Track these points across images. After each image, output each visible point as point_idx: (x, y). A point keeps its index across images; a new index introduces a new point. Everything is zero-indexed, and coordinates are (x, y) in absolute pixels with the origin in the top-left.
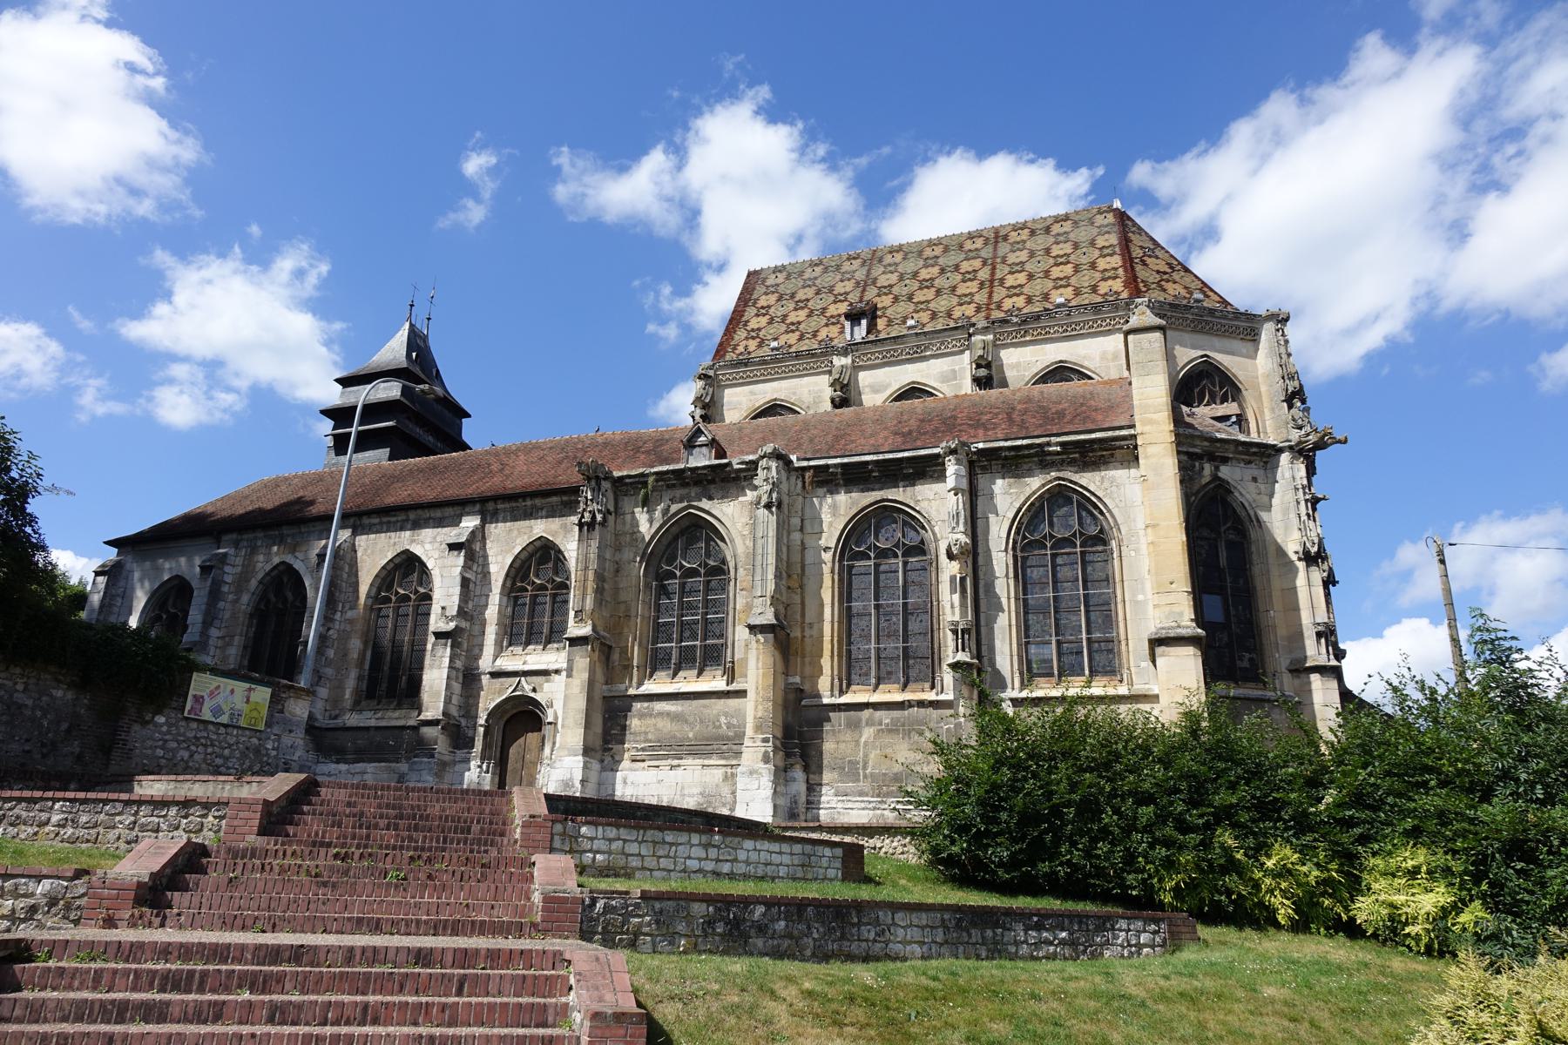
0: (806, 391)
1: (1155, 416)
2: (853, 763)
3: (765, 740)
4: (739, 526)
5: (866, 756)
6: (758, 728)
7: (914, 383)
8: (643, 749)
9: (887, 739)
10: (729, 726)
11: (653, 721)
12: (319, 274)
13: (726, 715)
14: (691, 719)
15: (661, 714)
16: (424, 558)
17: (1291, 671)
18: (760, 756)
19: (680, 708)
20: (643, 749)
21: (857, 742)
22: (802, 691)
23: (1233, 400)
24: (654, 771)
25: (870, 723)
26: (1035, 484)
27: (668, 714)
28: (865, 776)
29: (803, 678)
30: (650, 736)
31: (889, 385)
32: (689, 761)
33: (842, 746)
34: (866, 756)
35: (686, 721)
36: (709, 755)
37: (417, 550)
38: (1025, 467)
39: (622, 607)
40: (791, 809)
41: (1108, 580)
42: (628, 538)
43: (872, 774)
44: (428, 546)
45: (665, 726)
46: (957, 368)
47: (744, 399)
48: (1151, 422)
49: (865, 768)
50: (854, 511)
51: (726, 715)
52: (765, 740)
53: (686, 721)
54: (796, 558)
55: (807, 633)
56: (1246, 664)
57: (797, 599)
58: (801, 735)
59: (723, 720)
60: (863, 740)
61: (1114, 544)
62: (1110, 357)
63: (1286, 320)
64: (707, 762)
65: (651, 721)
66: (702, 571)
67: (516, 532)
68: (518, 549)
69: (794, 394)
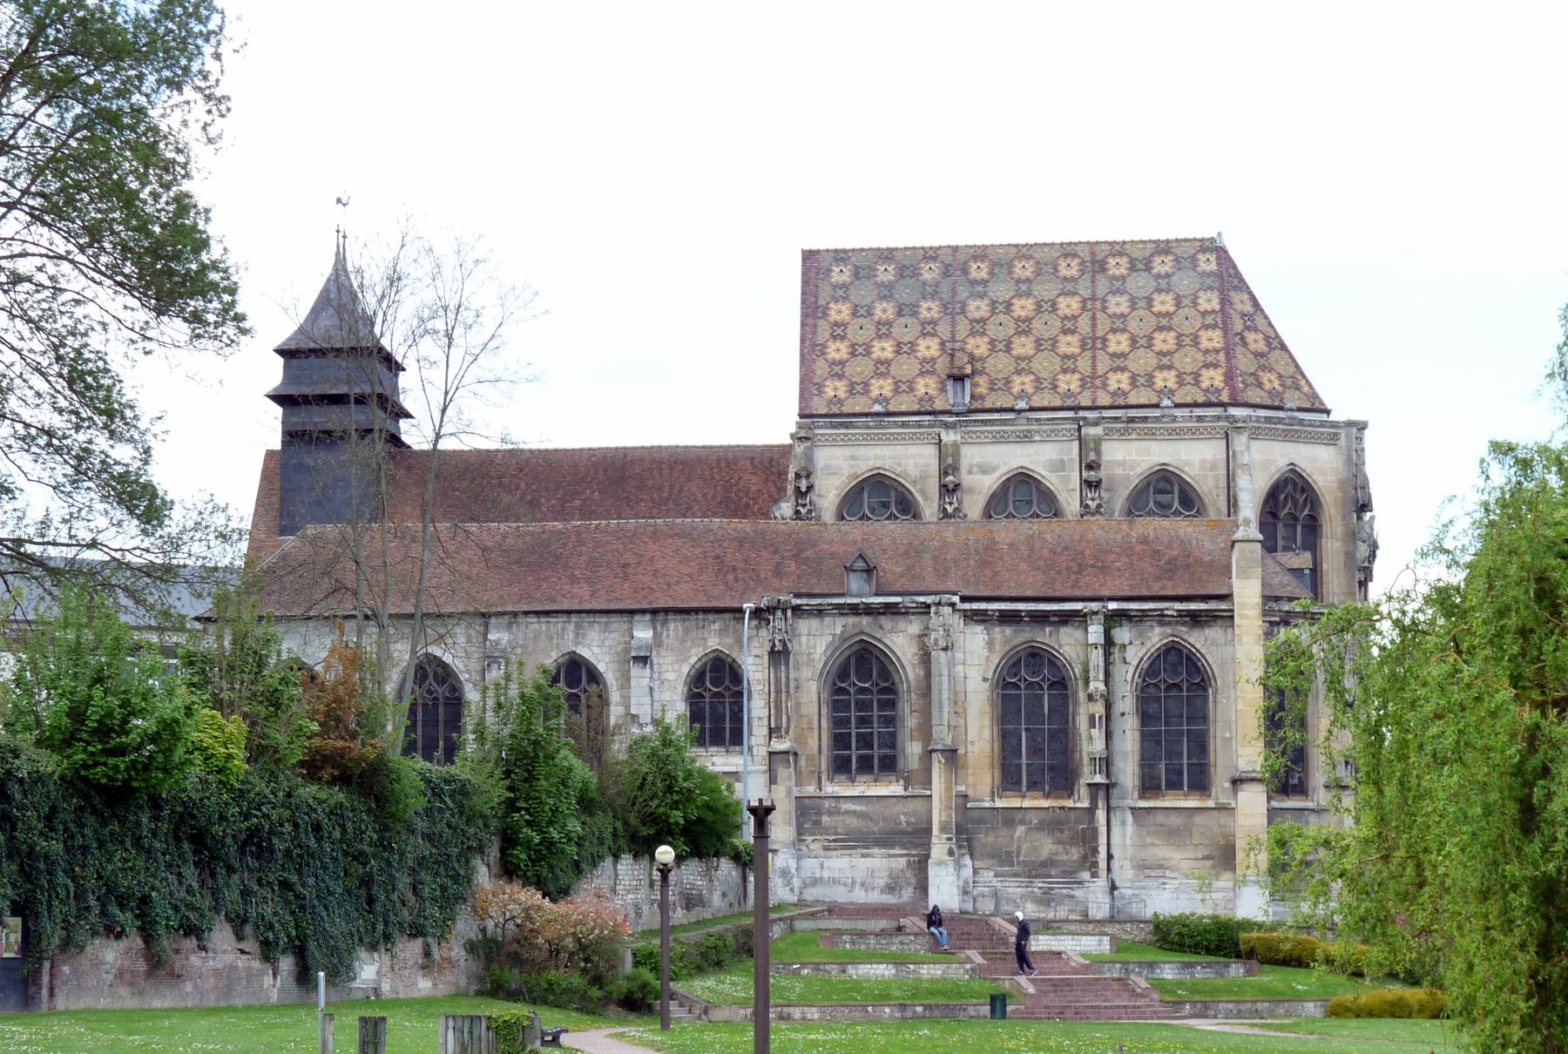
0: (911, 462)
1: (1250, 613)
2: (1009, 853)
3: (949, 839)
4: (909, 656)
5: (1019, 847)
6: (943, 829)
7: (1022, 467)
8: (834, 841)
9: (1037, 835)
10: (908, 823)
11: (841, 818)
12: (1249, 973)
13: (905, 814)
14: (875, 817)
15: (847, 812)
16: (592, 660)
17: (1326, 787)
18: (946, 851)
19: (864, 808)
20: (834, 841)
21: (1012, 838)
22: (966, 796)
23: (1305, 548)
24: (847, 859)
25: (1022, 822)
26: (1157, 637)
27: (854, 812)
28: (1018, 863)
29: (967, 786)
30: (839, 830)
31: (996, 469)
32: (876, 851)
33: (1000, 840)
34: (1019, 847)
35: (871, 819)
36: (892, 846)
37: (585, 652)
38: (1149, 624)
39: (805, 719)
40: (964, 887)
41: (1204, 718)
42: (805, 658)
43: (1024, 862)
44: (596, 650)
45: (853, 822)
46: (1065, 458)
47: (845, 464)
48: (1247, 617)
49: (1018, 856)
50: (1008, 648)
51: (905, 814)
52: (949, 839)
53: (871, 819)
54: (960, 688)
55: (969, 749)
56: (1295, 781)
57: (962, 721)
58: (967, 831)
59: (902, 818)
60: (1017, 834)
61: (1210, 691)
62: (1209, 466)
63: (1364, 428)
64: (891, 852)
65: (839, 818)
66: (875, 690)
67: (689, 644)
68: (694, 659)
69: (899, 464)
